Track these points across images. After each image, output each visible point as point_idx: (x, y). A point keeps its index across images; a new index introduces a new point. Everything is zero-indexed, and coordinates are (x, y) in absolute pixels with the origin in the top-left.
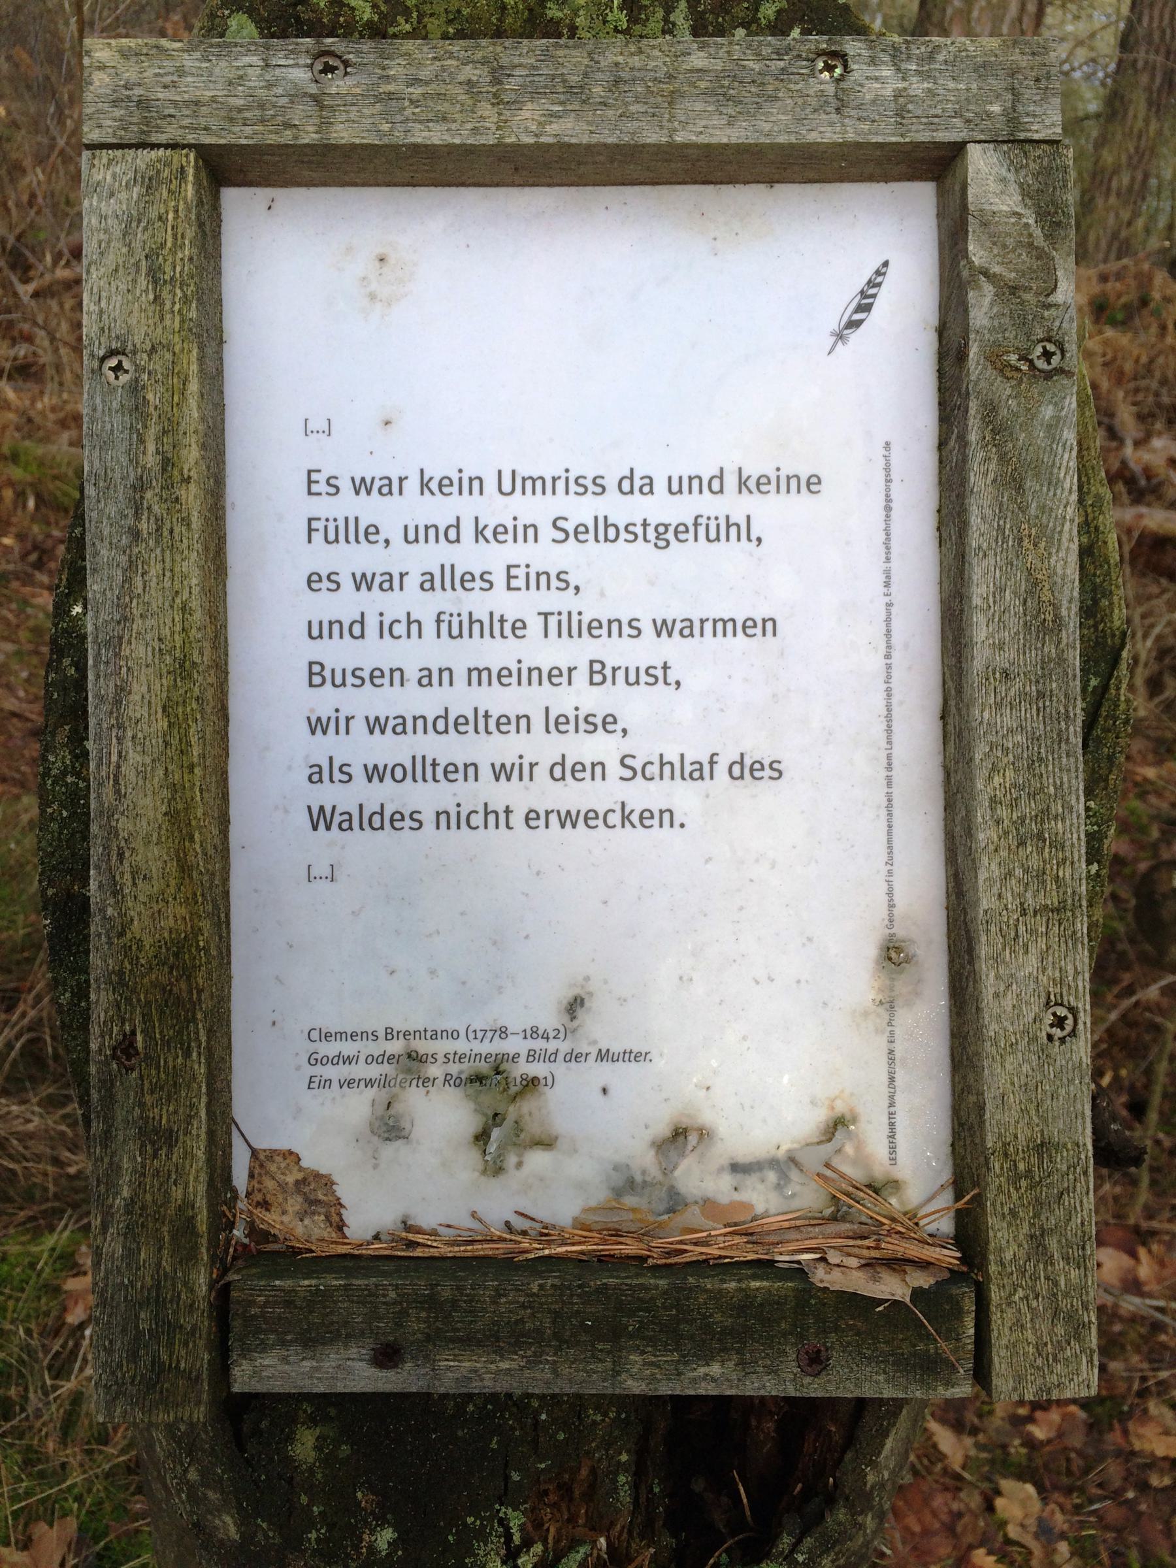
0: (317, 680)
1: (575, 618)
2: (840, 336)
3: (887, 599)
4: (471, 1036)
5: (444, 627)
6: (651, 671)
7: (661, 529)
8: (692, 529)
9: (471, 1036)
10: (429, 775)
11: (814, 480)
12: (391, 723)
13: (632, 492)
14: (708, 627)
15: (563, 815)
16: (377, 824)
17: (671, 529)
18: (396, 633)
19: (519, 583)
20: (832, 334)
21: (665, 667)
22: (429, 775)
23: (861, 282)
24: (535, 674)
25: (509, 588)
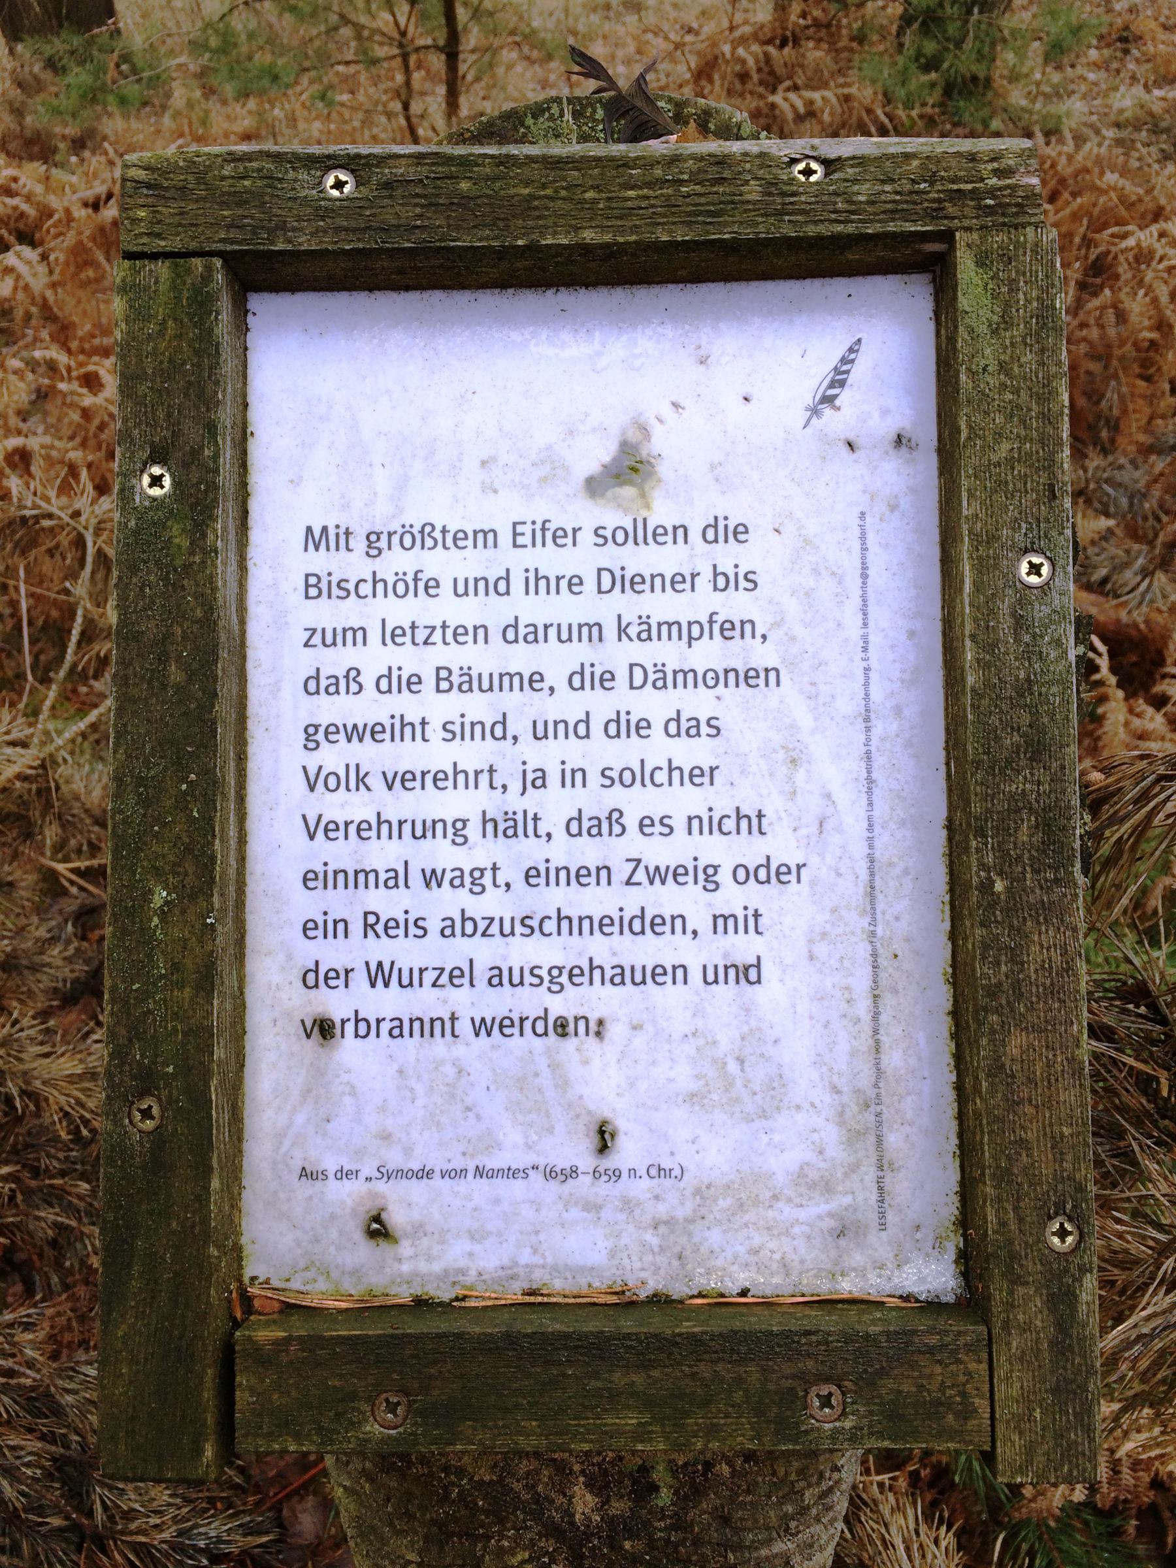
0: (313, 592)
1: (395, 674)
2: (815, 411)
3: (865, 664)
7: (477, 874)
8: (409, 632)
10: (530, 831)
12: (449, 876)
13: (318, 692)
16: (540, 1028)
17: (322, 730)
18: (362, 593)
19: (526, 540)
22: (530, 831)
23: (834, 360)
24: (478, 728)
25: (515, 545)
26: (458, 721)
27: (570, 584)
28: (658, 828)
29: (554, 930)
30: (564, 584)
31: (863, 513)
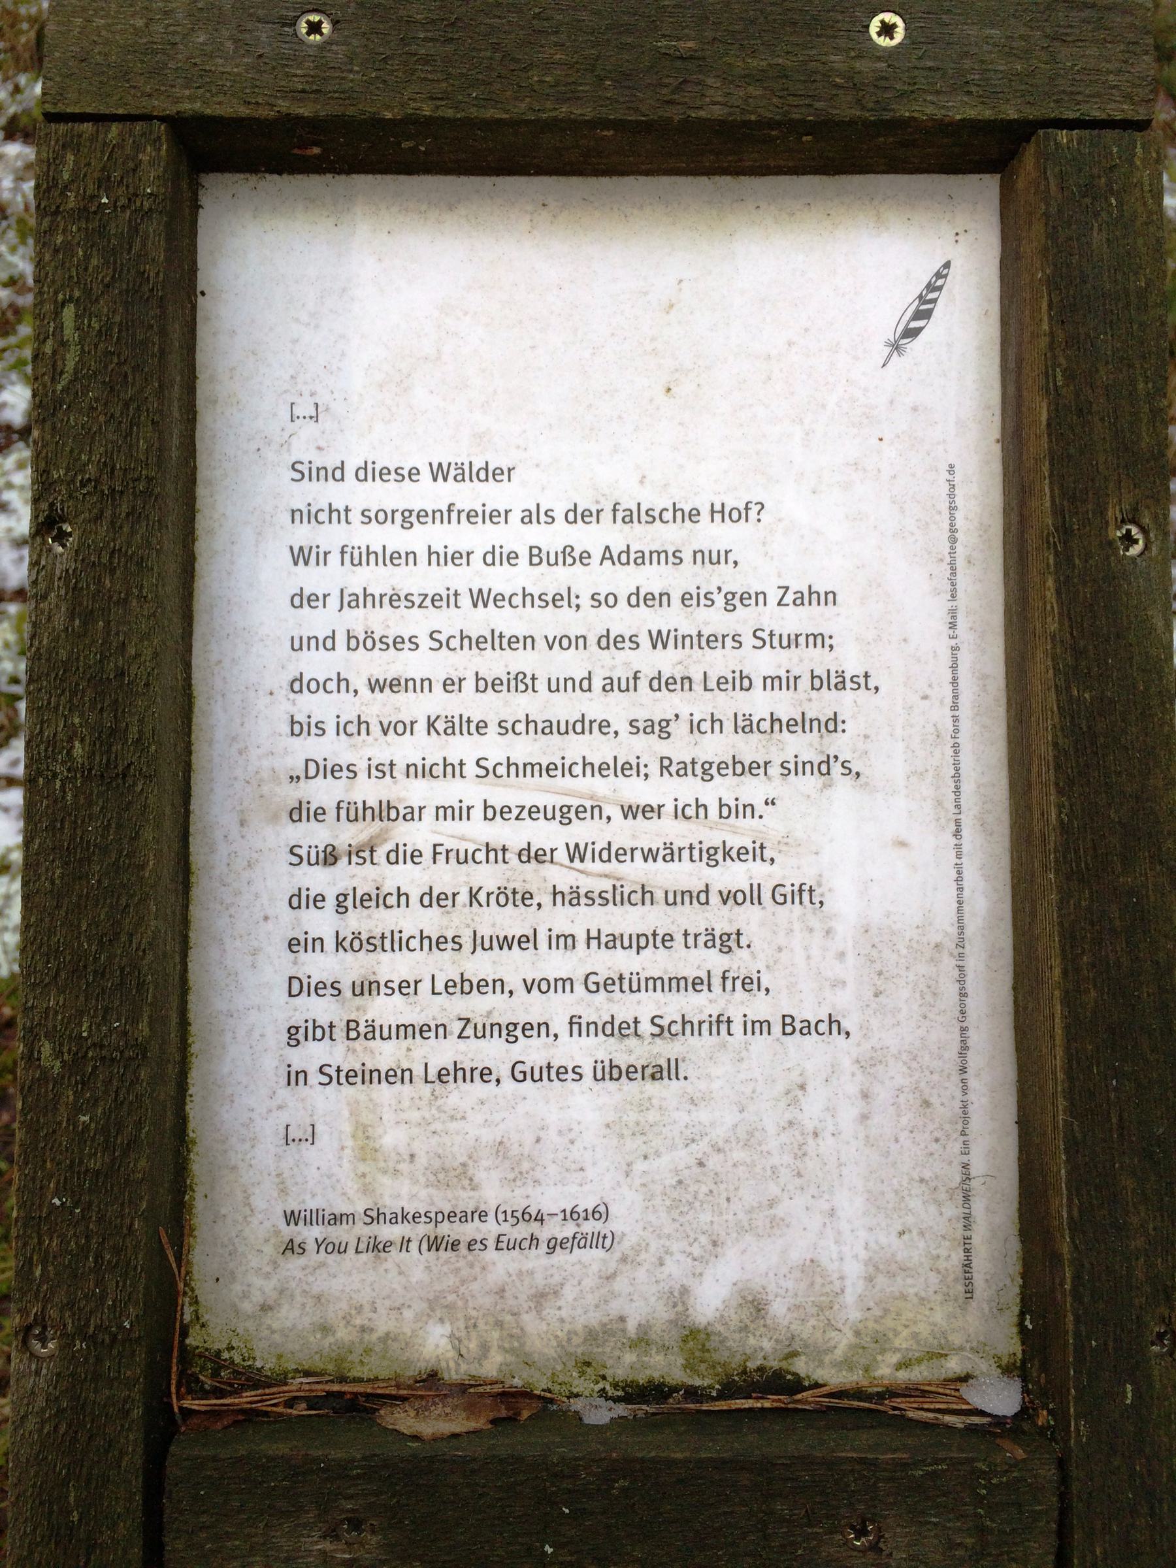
1: (304, 893)
3: (953, 642)
4: (501, 1217)
5: (347, 557)
6: (855, 679)
7: (565, 810)
8: (617, 982)
9: (501, 1217)
10: (497, 646)
11: (694, 512)
13: (628, 563)
14: (802, 640)
15: (646, 852)
20: (888, 344)
21: (866, 676)
22: (497, 646)
26: (793, 760)
27: (482, 1075)
28: (408, 645)
29: (335, 688)
30: (477, 1074)
31: (951, 466)
